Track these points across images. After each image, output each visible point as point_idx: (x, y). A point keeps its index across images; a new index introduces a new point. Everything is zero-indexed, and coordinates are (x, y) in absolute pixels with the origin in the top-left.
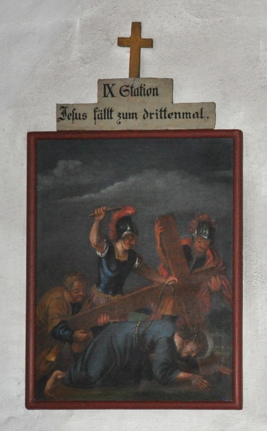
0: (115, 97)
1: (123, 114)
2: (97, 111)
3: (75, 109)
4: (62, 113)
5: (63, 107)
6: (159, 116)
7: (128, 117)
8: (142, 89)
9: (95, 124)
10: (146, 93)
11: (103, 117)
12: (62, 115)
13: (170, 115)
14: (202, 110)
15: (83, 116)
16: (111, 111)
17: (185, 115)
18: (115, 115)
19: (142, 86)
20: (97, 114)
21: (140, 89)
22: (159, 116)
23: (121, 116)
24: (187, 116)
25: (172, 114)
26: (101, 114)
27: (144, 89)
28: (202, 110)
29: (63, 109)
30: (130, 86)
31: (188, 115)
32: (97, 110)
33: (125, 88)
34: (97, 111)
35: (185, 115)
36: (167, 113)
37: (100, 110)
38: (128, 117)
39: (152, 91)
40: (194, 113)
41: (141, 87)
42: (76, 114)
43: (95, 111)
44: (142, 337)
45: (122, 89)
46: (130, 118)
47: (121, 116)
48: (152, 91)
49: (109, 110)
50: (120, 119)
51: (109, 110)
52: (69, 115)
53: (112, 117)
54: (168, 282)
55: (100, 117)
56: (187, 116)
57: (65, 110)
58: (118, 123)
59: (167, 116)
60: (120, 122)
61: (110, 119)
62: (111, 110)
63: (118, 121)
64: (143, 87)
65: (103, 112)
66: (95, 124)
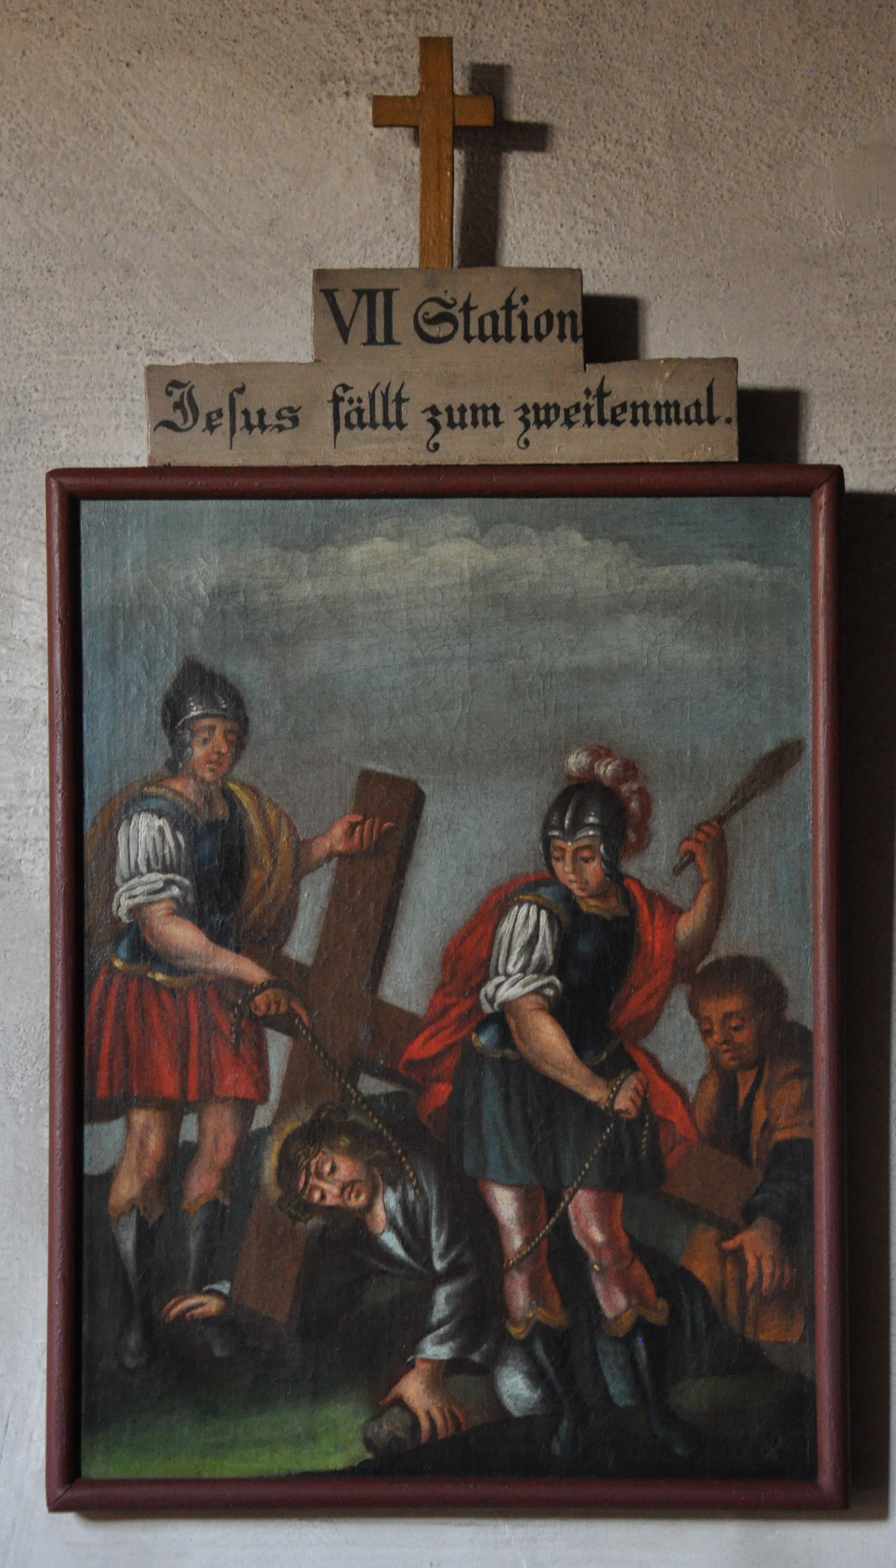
0: (399, 344)
1: (449, 409)
2: (342, 399)
3: (241, 390)
4: (178, 406)
5: (176, 384)
6: (594, 416)
7: (468, 419)
8: (515, 313)
9: (231, 448)
10: (531, 331)
11: (366, 418)
12: (179, 412)
13: (572, 411)
14: (710, 390)
15: (279, 416)
16: (400, 400)
17: (480, 414)
18: (413, 414)
19: (516, 300)
20: (344, 408)
21: (502, 314)
22: (594, 416)
23: (443, 419)
24: (462, 418)
25: (623, 407)
26: (360, 411)
27: (523, 317)
28: (710, 390)
29: (177, 393)
30: (460, 305)
31: (491, 413)
32: (347, 396)
33: (435, 309)
34: (342, 399)
35: (480, 414)
36: (608, 403)
37: (355, 399)
38: (468, 419)
39: (531, 331)
40: (567, 407)
41: (509, 306)
42: (246, 413)
43: (336, 400)
44: (186, 658)
45: (420, 314)
46: (475, 423)
47: (443, 419)
48: (556, 321)
49: (392, 396)
50: (525, 431)
51: (392, 396)
52: (572, 411)
53: (405, 419)
54: (701, 863)
55: (354, 418)
56: (462, 418)
57: (190, 394)
58: (522, 444)
59: (607, 415)
60: (527, 442)
61: (609, 426)
62: (399, 394)
63: (432, 442)
64: (516, 307)
65: (365, 405)
66: (231, 448)
